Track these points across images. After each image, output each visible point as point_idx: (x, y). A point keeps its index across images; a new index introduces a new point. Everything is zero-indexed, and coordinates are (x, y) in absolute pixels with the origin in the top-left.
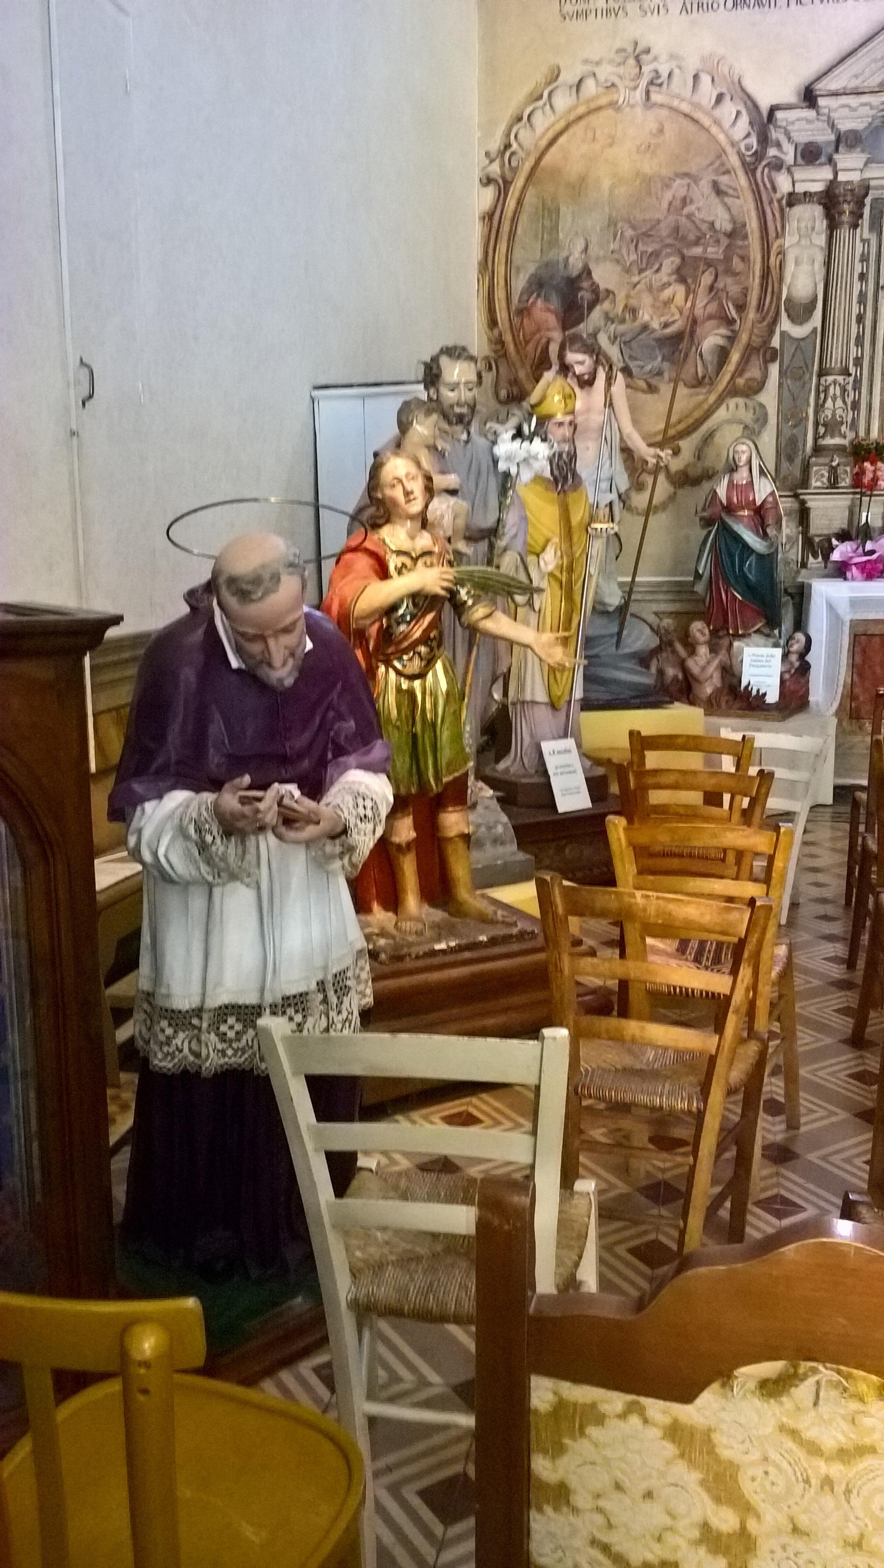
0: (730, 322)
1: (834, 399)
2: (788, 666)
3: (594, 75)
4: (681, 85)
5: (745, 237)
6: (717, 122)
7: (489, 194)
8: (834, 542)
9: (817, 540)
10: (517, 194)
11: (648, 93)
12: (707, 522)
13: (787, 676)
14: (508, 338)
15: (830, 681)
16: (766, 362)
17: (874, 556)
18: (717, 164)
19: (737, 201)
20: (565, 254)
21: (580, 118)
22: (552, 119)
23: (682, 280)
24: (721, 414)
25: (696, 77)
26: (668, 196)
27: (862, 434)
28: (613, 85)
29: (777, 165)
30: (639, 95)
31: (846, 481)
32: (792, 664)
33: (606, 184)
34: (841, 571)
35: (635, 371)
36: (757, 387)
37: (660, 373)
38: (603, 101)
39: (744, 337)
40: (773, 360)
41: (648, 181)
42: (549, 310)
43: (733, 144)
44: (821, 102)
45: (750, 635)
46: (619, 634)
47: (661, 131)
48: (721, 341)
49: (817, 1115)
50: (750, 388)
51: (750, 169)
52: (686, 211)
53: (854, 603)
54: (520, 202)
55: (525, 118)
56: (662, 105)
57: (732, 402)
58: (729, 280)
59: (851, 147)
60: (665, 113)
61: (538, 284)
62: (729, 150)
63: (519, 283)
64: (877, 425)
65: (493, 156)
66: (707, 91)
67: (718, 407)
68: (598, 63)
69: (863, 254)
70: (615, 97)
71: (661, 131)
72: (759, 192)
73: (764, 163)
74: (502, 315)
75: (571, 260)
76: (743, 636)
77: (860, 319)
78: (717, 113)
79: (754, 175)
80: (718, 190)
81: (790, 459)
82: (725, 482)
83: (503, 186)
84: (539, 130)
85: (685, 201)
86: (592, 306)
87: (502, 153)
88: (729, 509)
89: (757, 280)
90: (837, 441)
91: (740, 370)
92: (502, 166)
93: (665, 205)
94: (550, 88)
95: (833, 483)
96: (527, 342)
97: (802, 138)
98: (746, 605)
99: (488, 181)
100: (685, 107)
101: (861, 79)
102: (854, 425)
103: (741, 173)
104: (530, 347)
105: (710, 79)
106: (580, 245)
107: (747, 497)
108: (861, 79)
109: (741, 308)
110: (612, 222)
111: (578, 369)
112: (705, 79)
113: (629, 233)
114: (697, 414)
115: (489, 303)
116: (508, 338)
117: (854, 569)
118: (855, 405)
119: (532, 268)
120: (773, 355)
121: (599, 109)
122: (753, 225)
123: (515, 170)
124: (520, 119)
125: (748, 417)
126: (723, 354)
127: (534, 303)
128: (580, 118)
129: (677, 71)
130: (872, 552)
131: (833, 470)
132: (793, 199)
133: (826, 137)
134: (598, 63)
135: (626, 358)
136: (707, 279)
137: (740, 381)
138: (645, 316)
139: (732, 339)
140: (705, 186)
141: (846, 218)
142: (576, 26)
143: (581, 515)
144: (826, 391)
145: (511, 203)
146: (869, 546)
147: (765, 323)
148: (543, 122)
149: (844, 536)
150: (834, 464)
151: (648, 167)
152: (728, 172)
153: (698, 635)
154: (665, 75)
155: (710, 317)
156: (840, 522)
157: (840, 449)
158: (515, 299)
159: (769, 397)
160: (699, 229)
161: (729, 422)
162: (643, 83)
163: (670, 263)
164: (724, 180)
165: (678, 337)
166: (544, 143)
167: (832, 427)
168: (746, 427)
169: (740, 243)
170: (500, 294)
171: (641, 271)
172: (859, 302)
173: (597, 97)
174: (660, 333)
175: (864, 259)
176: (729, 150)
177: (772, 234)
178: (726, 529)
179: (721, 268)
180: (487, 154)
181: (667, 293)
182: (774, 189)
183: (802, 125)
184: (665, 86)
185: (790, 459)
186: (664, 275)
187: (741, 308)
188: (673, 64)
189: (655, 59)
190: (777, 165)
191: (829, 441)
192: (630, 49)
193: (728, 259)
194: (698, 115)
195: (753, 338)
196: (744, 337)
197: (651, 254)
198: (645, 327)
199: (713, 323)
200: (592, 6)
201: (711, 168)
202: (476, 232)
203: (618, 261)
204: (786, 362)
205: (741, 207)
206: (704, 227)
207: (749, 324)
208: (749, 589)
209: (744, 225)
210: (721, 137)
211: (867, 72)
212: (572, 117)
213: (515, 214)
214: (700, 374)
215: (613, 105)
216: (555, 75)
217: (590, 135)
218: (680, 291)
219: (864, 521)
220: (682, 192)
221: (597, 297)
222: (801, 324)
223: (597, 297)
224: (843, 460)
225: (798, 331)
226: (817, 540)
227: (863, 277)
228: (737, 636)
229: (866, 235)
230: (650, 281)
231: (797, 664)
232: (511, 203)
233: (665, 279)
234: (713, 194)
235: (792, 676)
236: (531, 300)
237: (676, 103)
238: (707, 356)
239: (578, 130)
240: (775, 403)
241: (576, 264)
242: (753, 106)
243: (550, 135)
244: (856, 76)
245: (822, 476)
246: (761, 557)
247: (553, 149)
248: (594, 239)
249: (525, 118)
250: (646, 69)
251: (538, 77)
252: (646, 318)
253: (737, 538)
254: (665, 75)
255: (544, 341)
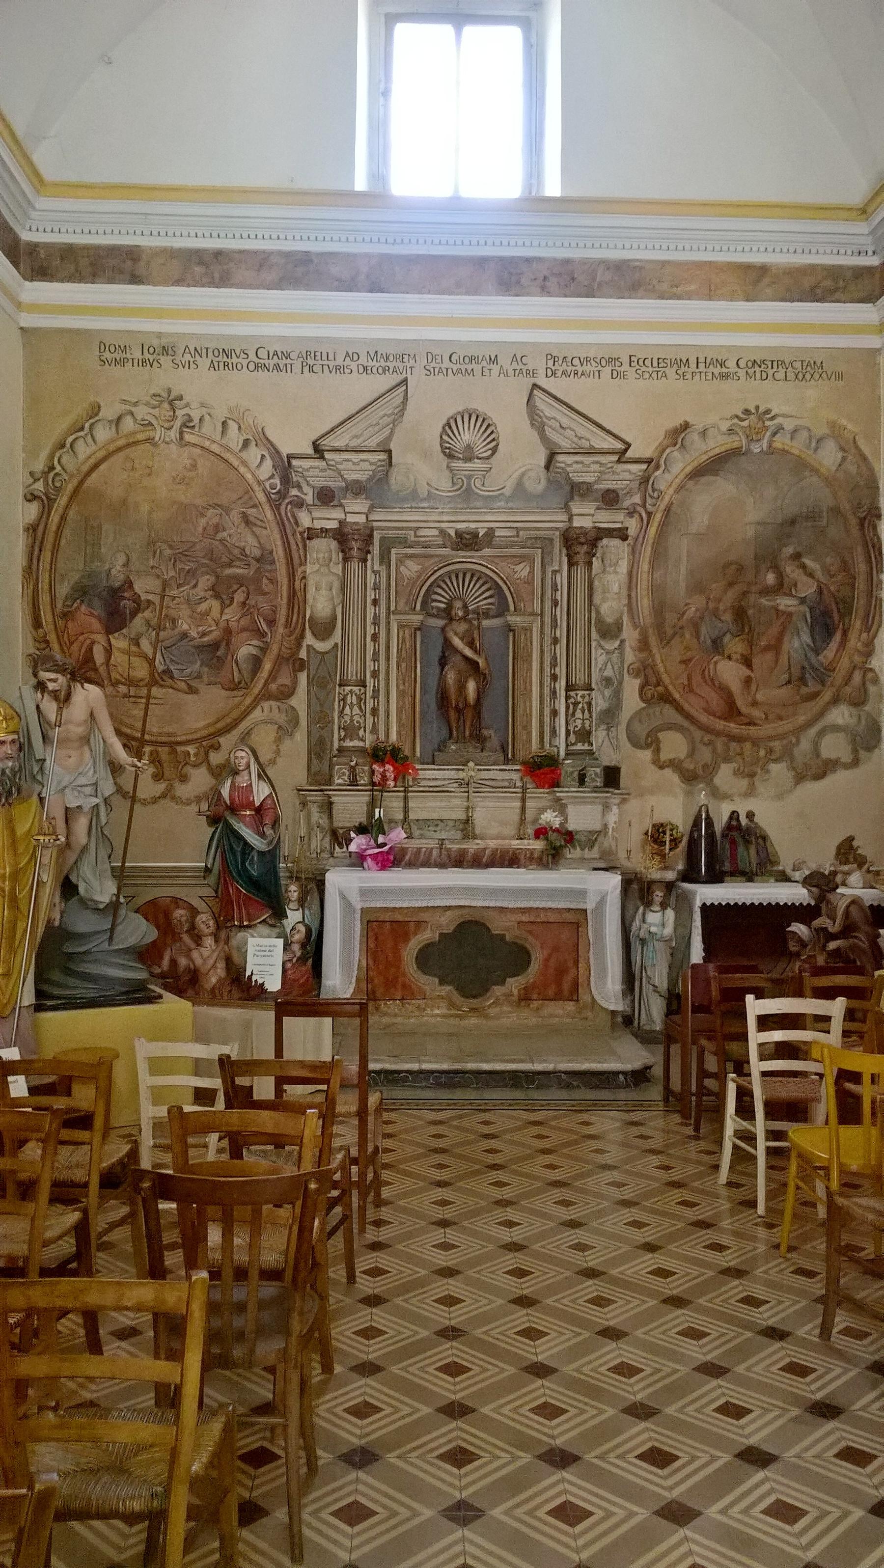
0: (261, 635)
1: (352, 706)
2: (289, 956)
3: (132, 414)
4: (211, 429)
5: (273, 562)
6: (244, 463)
7: (33, 510)
8: (353, 835)
9: (341, 831)
10: (61, 511)
11: (181, 433)
12: (214, 820)
13: (289, 965)
14: (52, 637)
15: (346, 964)
16: (295, 671)
17: (386, 848)
18: (246, 497)
19: (265, 532)
20: (107, 567)
21: (119, 449)
22: (94, 448)
23: (217, 596)
24: (257, 714)
25: (224, 424)
26: (203, 522)
27: (382, 737)
28: (150, 424)
29: (300, 504)
30: (173, 434)
31: (364, 780)
32: (294, 952)
33: (145, 508)
34: (359, 860)
35: (176, 673)
36: (287, 693)
37: (199, 676)
38: (141, 437)
39: (275, 648)
40: (301, 669)
41: (184, 508)
42: (92, 614)
43: (259, 483)
44: (327, 455)
45: (255, 925)
46: (112, 930)
47: (194, 466)
48: (254, 651)
49: (498, 1330)
50: (282, 693)
51: (275, 506)
52: (220, 536)
53: (364, 893)
54: (63, 518)
55: (68, 445)
56: (194, 445)
57: (266, 705)
58: (260, 598)
59: (357, 494)
60: (198, 451)
61: (82, 592)
62: (256, 488)
63: (63, 590)
64: (395, 729)
65: (37, 476)
66: (234, 438)
67: (254, 708)
68: (136, 404)
69: (375, 583)
70: (152, 434)
71: (194, 466)
72: (284, 525)
73: (287, 501)
74: (46, 617)
75: (113, 572)
76: (248, 927)
77: (375, 637)
78: (244, 455)
79: (278, 509)
80: (247, 520)
81: (320, 757)
82: (228, 784)
83: (46, 502)
84: (82, 456)
85: (218, 528)
86: (134, 614)
87: (45, 474)
88: (233, 809)
89: (285, 600)
90: (356, 743)
91: (273, 676)
92: (46, 484)
93: (200, 529)
94: (91, 421)
95: (354, 782)
96: (72, 643)
97: (320, 483)
98: (250, 898)
99: (31, 497)
100: (215, 448)
101: (362, 439)
102: (375, 730)
103: (267, 507)
104: (75, 647)
105: (236, 427)
106: (121, 559)
107: (248, 798)
108: (362, 439)
109: (271, 623)
110: (151, 543)
111: (51, 686)
112: (233, 426)
113: (168, 552)
114: (235, 714)
115: (34, 604)
116: (52, 637)
117: (369, 860)
118: (375, 711)
119: (75, 577)
120: (301, 665)
121: (136, 443)
122: (279, 553)
123: (58, 490)
124: (63, 446)
125: (282, 719)
126: (257, 662)
127: (78, 608)
128: (119, 449)
129: (207, 417)
130: (385, 845)
131: (352, 769)
132: (311, 534)
133: (335, 484)
134: (136, 404)
135: (168, 661)
136: (239, 597)
137: (273, 687)
138: (184, 625)
139: (264, 650)
140: (235, 515)
141: (355, 553)
142: (116, 371)
143: (28, 826)
144: (344, 700)
145: (55, 518)
146: (381, 839)
147: (293, 638)
148: (83, 450)
149: (362, 830)
150: (353, 764)
151: (183, 496)
152: (254, 506)
153: (203, 926)
154: (196, 421)
155: (244, 630)
156: (361, 818)
157: (362, 751)
158: (59, 605)
159: (299, 701)
160: (230, 552)
161: (266, 722)
162: (178, 424)
163: (205, 581)
164: (252, 512)
165: (215, 646)
166: (85, 468)
167: (350, 731)
168: (280, 727)
169: (269, 567)
170: (44, 599)
171: (179, 586)
172: (374, 624)
173: (134, 433)
174: (196, 642)
175: (376, 587)
176: (256, 488)
177: (296, 561)
178: (228, 826)
179: (251, 588)
180: (32, 474)
181: (204, 607)
182: (298, 525)
183: (316, 472)
184: (197, 429)
185: (320, 757)
186: (200, 591)
187: (271, 623)
188: (204, 411)
189: (187, 405)
190: (300, 504)
191: (348, 743)
192: (165, 395)
193: (257, 580)
194: (227, 456)
195: (283, 649)
196: (275, 648)
197: (188, 572)
198: (184, 635)
199: (245, 635)
200: (128, 356)
201: (240, 502)
202: (20, 544)
203: (158, 577)
204: (312, 673)
205: (268, 536)
206: (236, 552)
207: (279, 637)
208: (254, 884)
209: (271, 552)
210: (249, 476)
211: (367, 434)
212: (112, 448)
213: (58, 528)
214: (236, 680)
215: (149, 440)
216: (95, 410)
217: (129, 465)
218: (216, 605)
219: (377, 816)
220: (215, 520)
221: (139, 606)
222: (323, 640)
223: (139, 606)
224: (361, 761)
225: (322, 646)
226: (341, 831)
227: (375, 602)
228: (241, 927)
229: (376, 568)
230: (188, 595)
231: (298, 954)
232: (55, 518)
233: (202, 594)
234: (243, 525)
235: (294, 965)
236: (75, 605)
237: (207, 444)
238: (243, 666)
239: (119, 458)
240: (304, 706)
241: (118, 576)
242: (275, 452)
243: (92, 461)
244: (356, 437)
245: (344, 774)
246: (261, 854)
247: (94, 475)
248: (134, 557)
249: (68, 445)
250: (179, 413)
251: (79, 410)
252: (185, 627)
253: (240, 838)
254: (196, 421)
255: (88, 642)
